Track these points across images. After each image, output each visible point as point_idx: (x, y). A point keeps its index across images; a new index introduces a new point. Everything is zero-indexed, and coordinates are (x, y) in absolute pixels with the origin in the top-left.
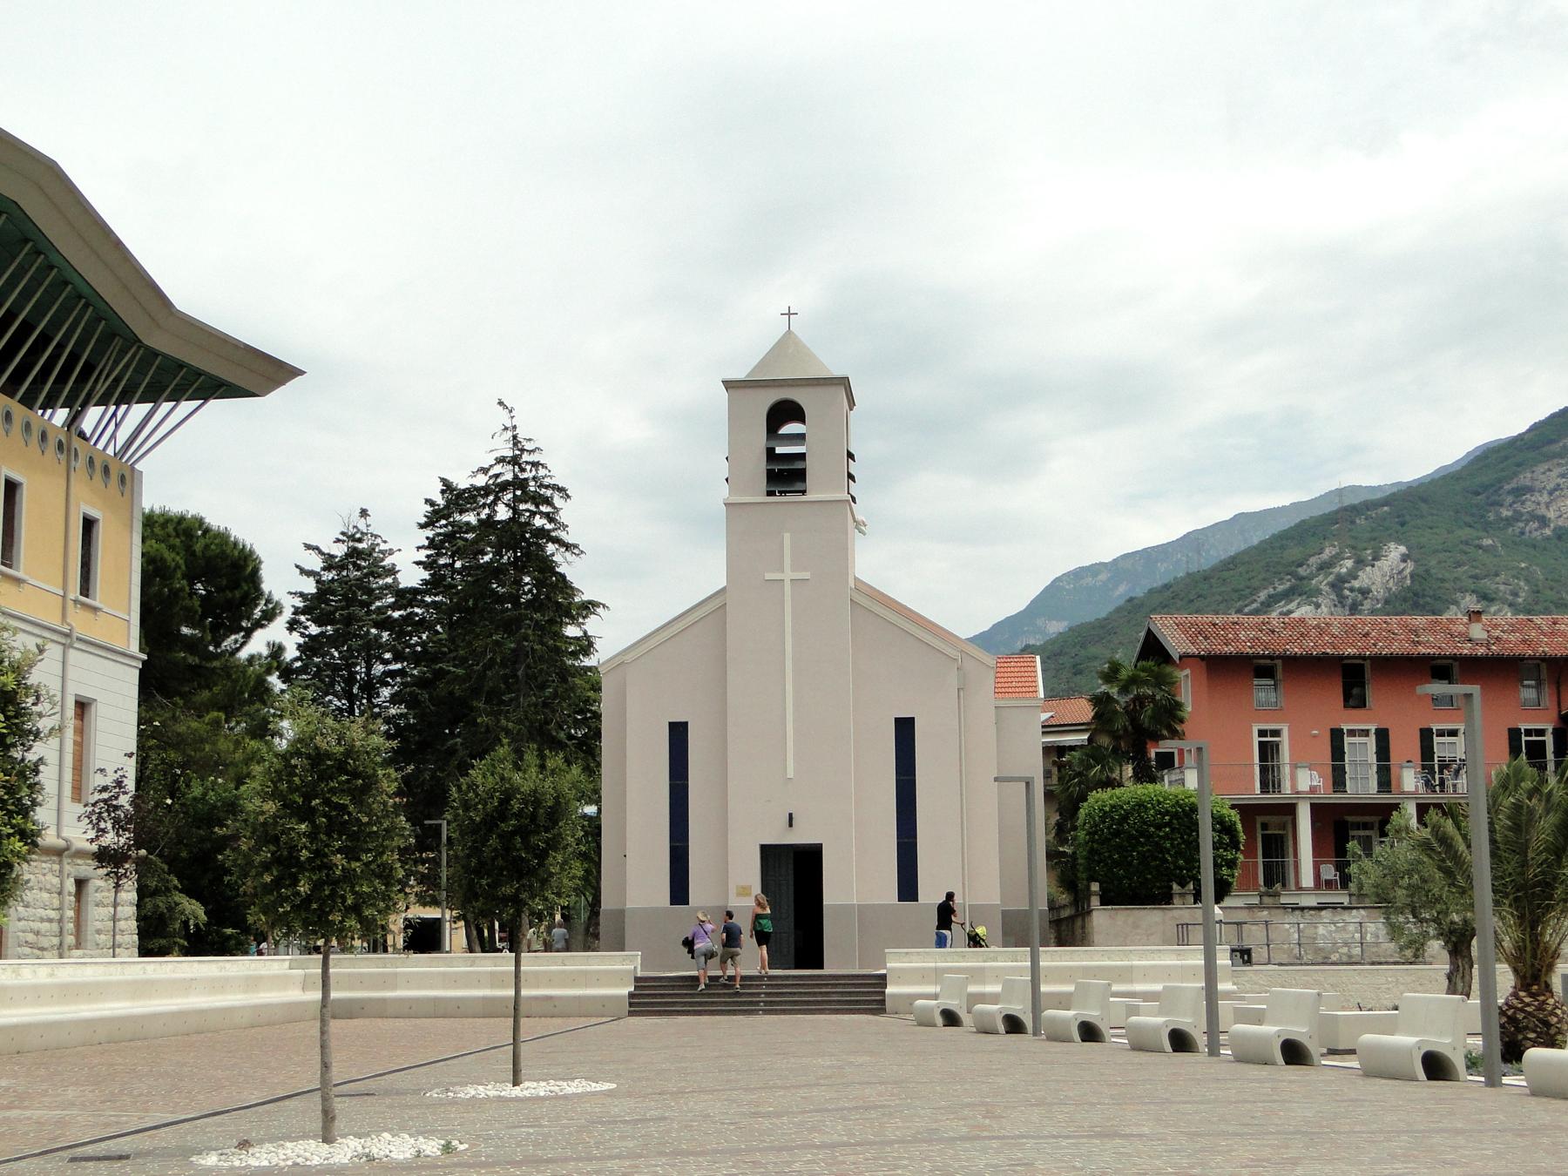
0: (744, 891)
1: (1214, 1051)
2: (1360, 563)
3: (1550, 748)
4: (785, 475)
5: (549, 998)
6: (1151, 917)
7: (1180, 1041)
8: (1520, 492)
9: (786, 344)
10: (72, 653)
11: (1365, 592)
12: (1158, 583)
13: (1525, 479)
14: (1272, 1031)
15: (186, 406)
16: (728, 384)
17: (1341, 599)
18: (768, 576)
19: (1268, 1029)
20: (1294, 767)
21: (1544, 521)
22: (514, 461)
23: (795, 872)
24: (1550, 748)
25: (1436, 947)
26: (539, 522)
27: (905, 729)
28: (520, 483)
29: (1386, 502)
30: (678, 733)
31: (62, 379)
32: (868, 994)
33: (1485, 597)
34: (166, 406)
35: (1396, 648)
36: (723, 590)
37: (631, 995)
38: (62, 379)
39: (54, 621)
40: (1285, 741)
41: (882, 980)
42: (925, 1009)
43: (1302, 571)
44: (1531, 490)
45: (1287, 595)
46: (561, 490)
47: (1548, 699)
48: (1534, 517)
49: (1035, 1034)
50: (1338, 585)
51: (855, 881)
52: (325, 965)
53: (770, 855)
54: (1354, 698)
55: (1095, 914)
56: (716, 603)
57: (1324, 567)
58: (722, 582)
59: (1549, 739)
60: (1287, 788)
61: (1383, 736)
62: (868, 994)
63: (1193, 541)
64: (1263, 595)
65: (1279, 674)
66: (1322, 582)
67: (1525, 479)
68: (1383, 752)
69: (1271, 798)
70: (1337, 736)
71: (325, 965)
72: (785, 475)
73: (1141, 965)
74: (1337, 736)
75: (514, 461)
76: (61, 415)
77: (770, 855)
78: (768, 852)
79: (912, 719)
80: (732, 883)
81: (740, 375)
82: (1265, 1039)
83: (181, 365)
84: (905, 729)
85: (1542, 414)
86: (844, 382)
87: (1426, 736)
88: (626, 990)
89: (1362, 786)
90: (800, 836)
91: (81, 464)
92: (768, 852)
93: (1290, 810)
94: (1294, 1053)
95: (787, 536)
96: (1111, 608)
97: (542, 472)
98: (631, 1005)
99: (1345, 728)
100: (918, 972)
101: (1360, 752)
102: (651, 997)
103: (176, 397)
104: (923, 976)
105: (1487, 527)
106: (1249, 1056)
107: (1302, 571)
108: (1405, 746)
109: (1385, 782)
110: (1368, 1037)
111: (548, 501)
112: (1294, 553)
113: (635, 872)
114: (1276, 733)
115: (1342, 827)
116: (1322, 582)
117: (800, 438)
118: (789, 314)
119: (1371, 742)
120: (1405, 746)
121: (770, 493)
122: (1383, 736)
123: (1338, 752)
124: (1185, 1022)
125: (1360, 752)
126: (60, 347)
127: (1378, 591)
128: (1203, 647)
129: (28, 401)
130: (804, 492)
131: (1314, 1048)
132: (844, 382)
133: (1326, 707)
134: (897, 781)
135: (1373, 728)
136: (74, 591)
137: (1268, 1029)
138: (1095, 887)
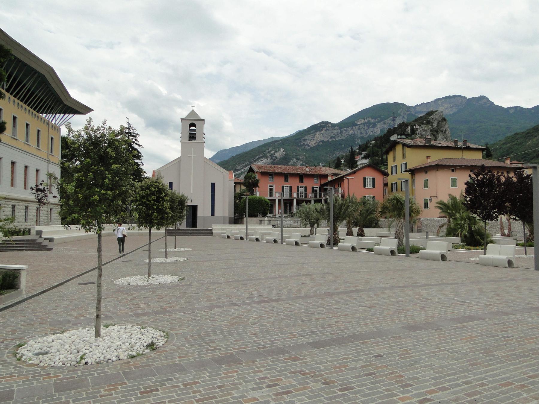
1: (247, 240)
2: (276, 152)
3: (318, 192)
4: (192, 137)
6: (254, 219)
7: (242, 238)
8: (305, 140)
10: (50, 165)
11: (276, 157)
12: (238, 154)
13: (306, 138)
14: (293, 240)
15: (71, 115)
16: (182, 119)
17: (272, 158)
19: (254, 237)
20: (276, 193)
21: (309, 146)
22: (129, 128)
24: (318, 192)
25: (308, 225)
26: (134, 140)
27: (213, 185)
28: (130, 133)
29: (281, 140)
31: (44, 109)
32: (209, 233)
33: (298, 159)
34: (67, 115)
35: (294, 172)
38: (44, 109)
39: (46, 158)
40: (274, 188)
42: (236, 237)
43: (265, 153)
44: (306, 140)
45: (262, 157)
46: (138, 134)
47: (319, 182)
48: (307, 145)
49: (282, 243)
50: (271, 156)
51: (203, 212)
52: (150, 230)
54: (286, 180)
56: (179, 160)
57: (269, 152)
58: (178, 155)
59: (318, 189)
60: (274, 196)
61: (291, 187)
62: (209, 233)
63: (245, 146)
64: (258, 157)
66: (269, 155)
67: (306, 138)
68: (291, 190)
69: (271, 198)
70: (283, 187)
71: (150, 230)
72: (192, 137)
73: (258, 227)
74: (283, 187)
75: (129, 128)
76: (44, 115)
81: (183, 117)
82: (253, 238)
83: (71, 108)
84: (213, 185)
86: (204, 120)
87: (298, 188)
89: (287, 196)
91: (50, 127)
93: (275, 200)
94: (257, 240)
96: (229, 157)
97: (134, 131)
100: (217, 228)
101: (287, 190)
103: (69, 114)
104: (219, 229)
105: (299, 146)
106: (289, 244)
107: (265, 153)
108: (294, 190)
109: (291, 196)
110: (311, 241)
111: (136, 137)
112: (264, 149)
114: (272, 186)
115: (288, 203)
116: (269, 155)
117: (195, 130)
120: (294, 190)
122: (291, 187)
123: (283, 190)
124: (276, 238)
125: (287, 190)
126: (48, 104)
127: (279, 157)
128: (260, 170)
129: (38, 112)
131: (260, 239)
132: (204, 120)
133: (280, 181)
136: (50, 153)
137: (254, 237)
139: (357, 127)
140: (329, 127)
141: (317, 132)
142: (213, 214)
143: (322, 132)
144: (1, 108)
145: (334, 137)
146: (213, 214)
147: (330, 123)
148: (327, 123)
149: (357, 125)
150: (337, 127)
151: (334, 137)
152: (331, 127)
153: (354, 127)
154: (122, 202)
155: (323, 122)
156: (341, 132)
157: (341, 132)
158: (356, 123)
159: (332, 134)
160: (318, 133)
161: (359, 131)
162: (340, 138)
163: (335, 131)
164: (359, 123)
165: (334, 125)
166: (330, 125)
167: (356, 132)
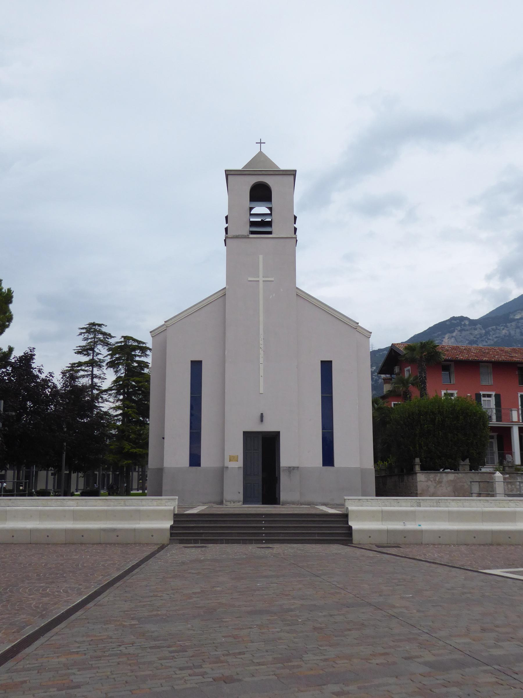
0: (233, 459)
5: (114, 530)
9: (260, 157)
16: (228, 174)
18: (250, 279)
23: (264, 448)
27: (326, 367)
30: (196, 367)
36: (225, 288)
37: (172, 527)
41: (345, 517)
53: (249, 437)
55: (418, 475)
58: (223, 285)
65: (452, 369)
77: (249, 437)
78: (248, 436)
79: (331, 362)
80: (226, 451)
81: (239, 166)
84: (326, 367)
85: (432, 325)
86: (293, 173)
88: (167, 524)
90: (268, 427)
92: (248, 436)
95: (261, 257)
98: (171, 534)
99: (482, 393)
102: (187, 529)
104: (372, 516)
113: (170, 446)
118: (261, 143)
119: (493, 400)
121: (252, 233)
130: (270, 233)
134: (322, 397)
135: (493, 393)
138: (417, 460)
139: (513, 324)
140: (465, 325)
141: (445, 334)
142: (328, 458)
143: (454, 334)
144: (1, 278)
145: (475, 342)
146: (328, 458)
147: (467, 318)
148: (462, 319)
149: (514, 320)
150: (479, 326)
151: (475, 342)
152: (469, 325)
153: (509, 325)
154: (38, 382)
155: (453, 318)
156: (487, 333)
157: (487, 333)
158: (511, 317)
159: (472, 337)
160: (447, 336)
161: (518, 331)
162: (485, 343)
163: (476, 332)
164: (516, 318)
165: (473, 323)
166: (467, 323)
167: (512, 332)
